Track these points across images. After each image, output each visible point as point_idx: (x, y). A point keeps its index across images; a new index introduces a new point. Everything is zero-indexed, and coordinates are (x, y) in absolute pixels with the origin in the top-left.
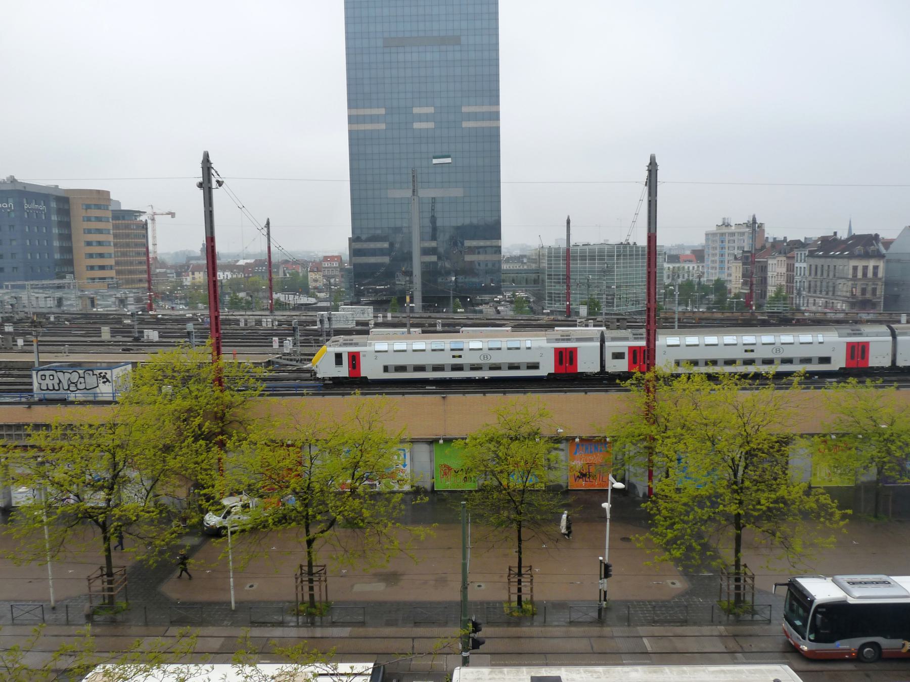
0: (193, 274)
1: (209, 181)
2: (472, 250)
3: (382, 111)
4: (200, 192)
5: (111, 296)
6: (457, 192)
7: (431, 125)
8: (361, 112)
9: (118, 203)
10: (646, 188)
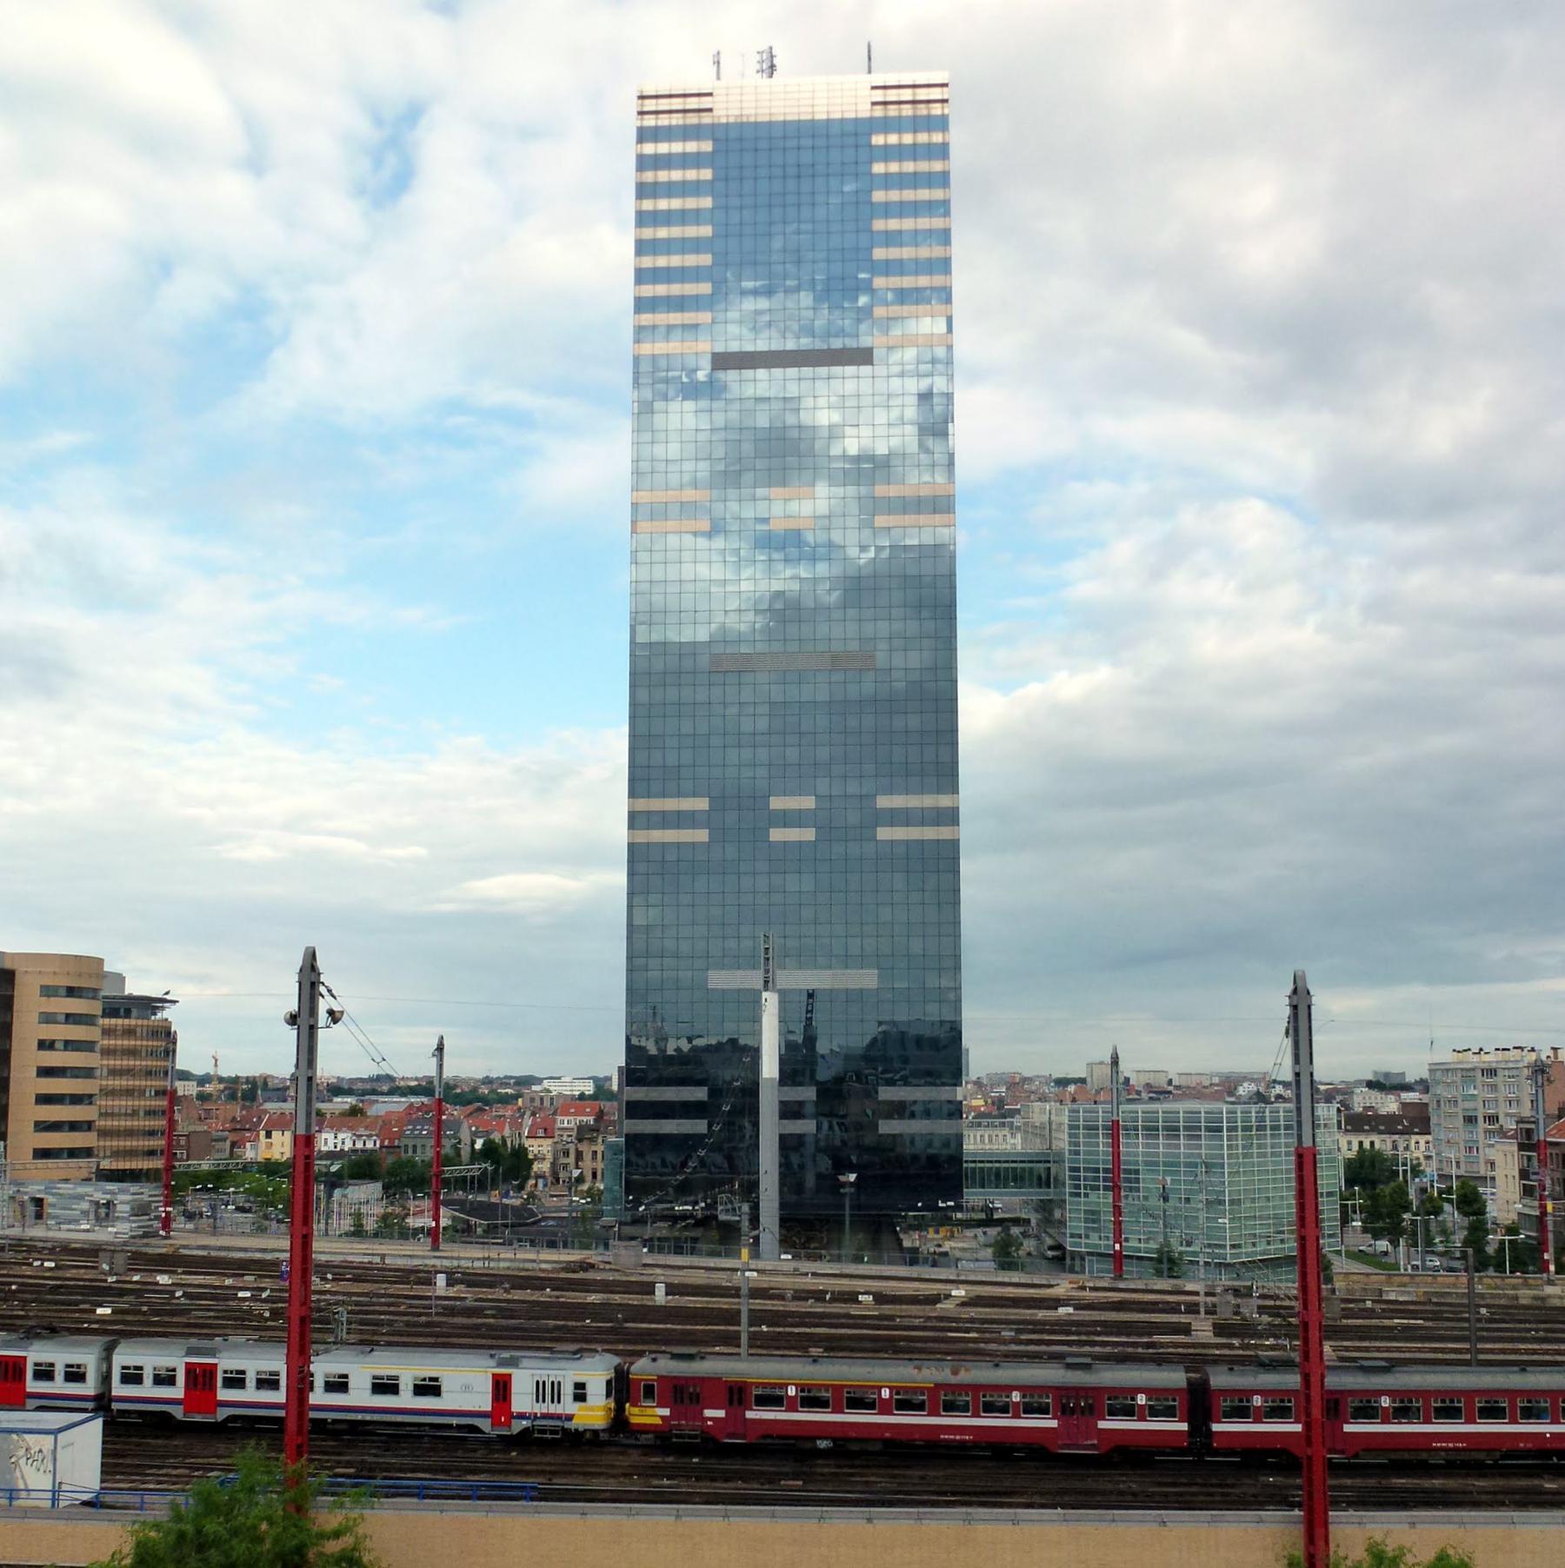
0: (269, 1135)
1: (313, 1011)
2: (900, 1110)
3: (702, 804)
4: (292, 1033)
5: (81, 1197)
6: (866, 979)
7: (809, 834)
8: (656, 804)
9: (120, 979)
10: (1288, 1044)
